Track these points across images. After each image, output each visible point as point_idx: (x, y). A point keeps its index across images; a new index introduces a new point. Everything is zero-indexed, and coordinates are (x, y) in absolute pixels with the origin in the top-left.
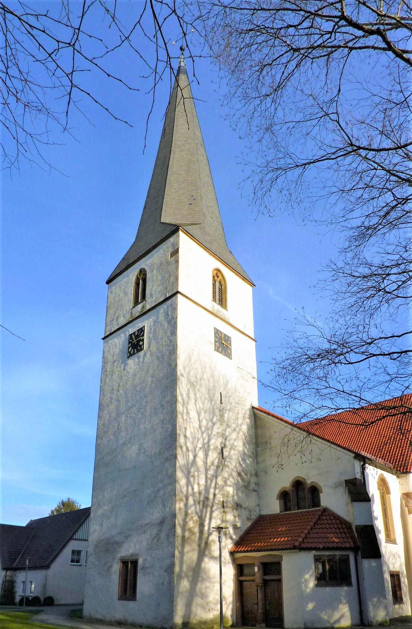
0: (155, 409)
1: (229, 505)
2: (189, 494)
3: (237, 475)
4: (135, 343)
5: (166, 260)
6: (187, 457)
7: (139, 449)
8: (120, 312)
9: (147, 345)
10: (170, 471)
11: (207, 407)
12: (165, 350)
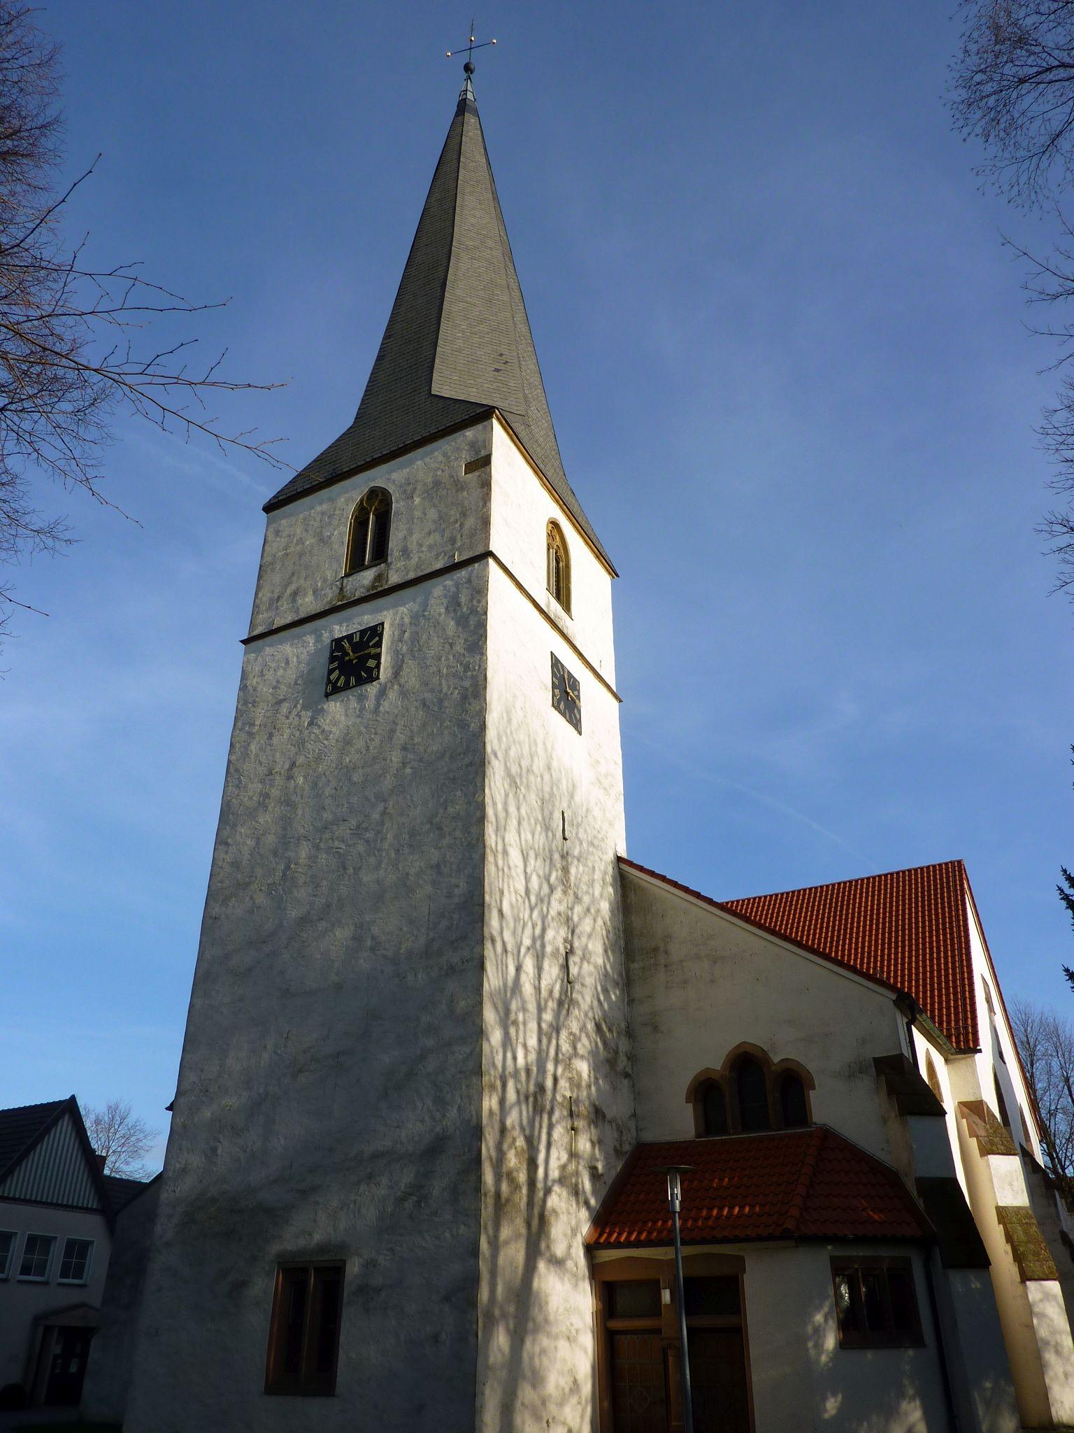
0: (413, 833)
1: (582, 1108)
2: (507, 1073)
3: (595, 1029)
4: (351, 661)
5: (451, 476)
6: (504, 968)
7: (354, 938)
8: (302, 581)
9: (390, 671)
10: (462, 1004)
11: (539, 842)
12: (449, 688)
